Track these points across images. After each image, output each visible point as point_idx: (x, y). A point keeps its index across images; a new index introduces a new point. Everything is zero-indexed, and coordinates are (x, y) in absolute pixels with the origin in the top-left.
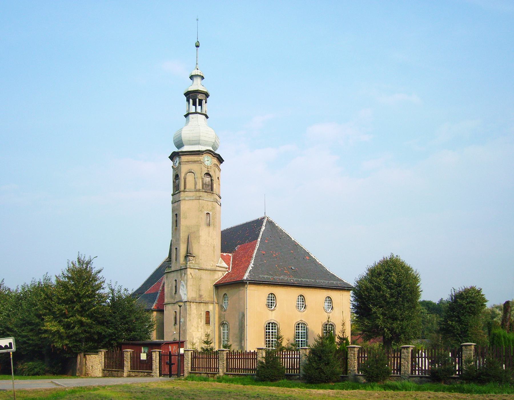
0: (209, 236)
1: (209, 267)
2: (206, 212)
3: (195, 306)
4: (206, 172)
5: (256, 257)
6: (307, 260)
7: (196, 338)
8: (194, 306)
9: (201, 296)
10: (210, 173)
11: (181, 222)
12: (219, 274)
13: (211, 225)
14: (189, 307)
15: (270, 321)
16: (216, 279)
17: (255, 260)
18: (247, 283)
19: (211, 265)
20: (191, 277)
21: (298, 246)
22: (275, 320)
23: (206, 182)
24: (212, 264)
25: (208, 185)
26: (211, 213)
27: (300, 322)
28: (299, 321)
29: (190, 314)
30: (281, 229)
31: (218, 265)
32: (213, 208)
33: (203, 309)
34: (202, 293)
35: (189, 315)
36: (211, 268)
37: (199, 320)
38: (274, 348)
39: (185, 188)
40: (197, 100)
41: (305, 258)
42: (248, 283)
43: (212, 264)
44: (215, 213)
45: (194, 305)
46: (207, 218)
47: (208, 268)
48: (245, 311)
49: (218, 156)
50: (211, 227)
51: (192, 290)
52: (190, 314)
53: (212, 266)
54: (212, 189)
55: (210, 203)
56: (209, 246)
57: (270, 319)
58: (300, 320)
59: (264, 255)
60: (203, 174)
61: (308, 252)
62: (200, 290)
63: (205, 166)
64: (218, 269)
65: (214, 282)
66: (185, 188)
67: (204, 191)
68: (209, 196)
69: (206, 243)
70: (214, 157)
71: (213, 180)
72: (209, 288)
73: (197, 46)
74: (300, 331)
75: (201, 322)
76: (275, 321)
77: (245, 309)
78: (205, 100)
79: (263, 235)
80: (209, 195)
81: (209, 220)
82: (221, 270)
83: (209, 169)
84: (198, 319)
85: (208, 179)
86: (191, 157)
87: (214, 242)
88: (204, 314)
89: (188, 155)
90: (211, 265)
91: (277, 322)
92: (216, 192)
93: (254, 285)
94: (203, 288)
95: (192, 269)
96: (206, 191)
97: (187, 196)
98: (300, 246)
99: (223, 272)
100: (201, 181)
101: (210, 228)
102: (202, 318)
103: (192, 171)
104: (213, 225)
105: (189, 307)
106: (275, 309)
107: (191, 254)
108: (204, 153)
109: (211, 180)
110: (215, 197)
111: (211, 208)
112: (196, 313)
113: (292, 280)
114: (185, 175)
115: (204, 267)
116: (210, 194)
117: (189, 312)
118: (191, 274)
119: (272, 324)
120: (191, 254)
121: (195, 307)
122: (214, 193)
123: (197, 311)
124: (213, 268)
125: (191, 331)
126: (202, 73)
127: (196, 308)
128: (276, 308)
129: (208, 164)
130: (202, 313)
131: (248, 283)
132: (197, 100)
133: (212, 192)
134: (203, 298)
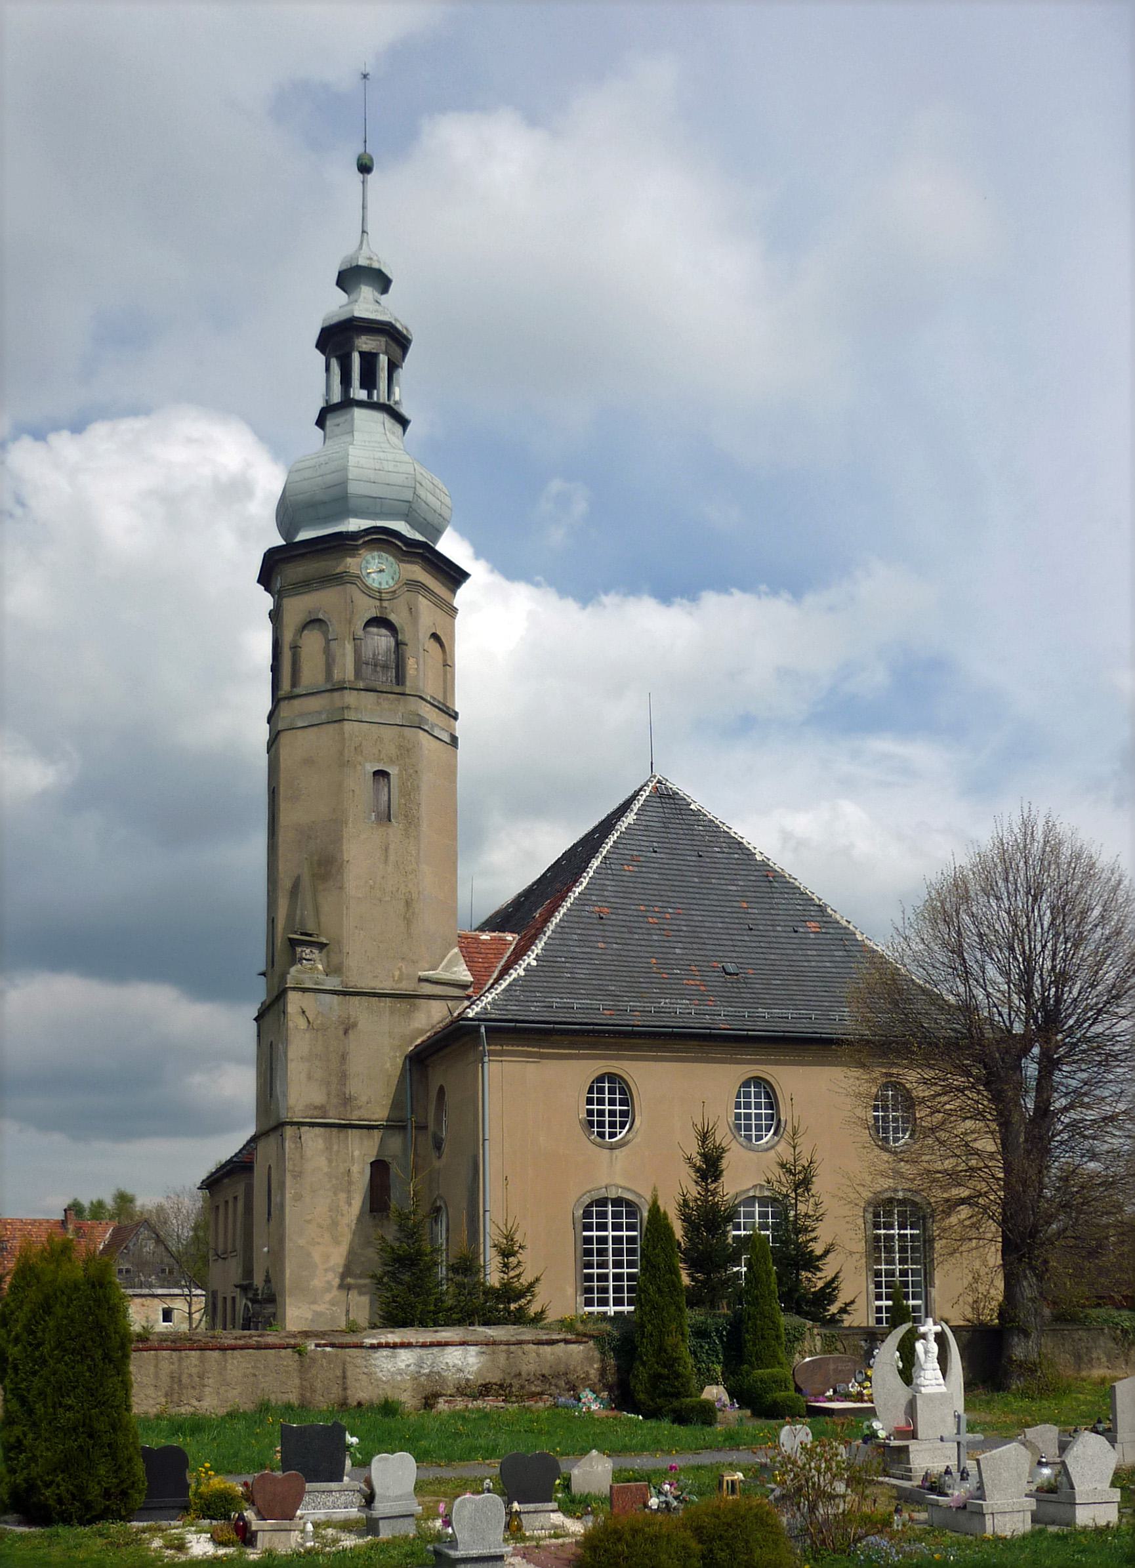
0: (386, 861)
1: (386, 986)
2: (371, 768)
3: (320, 1141)
4: (374, 613)
5: (559, 930)
6: (812, 936)
7: (326, 1270)
8: (314, 1140)
9: (347, 1101)
10: (392, 617)
11: (281, 818)
12: (433, 1011)
13: (396, 818)
14: (293, 1146)
15: (603, 1193)
16: (418, 1029)
17: (551, 944)
18: (478, 1031)
19: (393, 977)
20: (302, 1023)
21: (776, 884)
22: (627, 1185)
23: (374, 655)
24: (400, 969)
25: (385, 667)
26: (393, 771)
27: (751, 1194)
28: (748, 1190)
29: (301, 1172)
30: (712, 821)
31: (439, 973)
32: (406, 752)
33: (356, 1153)
34: (355, 1087)
35: (295, 1177)
36: (396, 986)
37: (342, 1196)
38: (626, 1309)
39: (295, 683)
40: (356, 359)
41: (801, 930)
42: (483, 1030)
43: (400, 969)
44: (412, 771)
45: (316, 1136)
46: (377, 792)
47: (381, 986)
48: (481, 1152)
49: (421, 551)
50: (397, 826)
51: (309, 1078)
52: (298, 1175)
53: (400, 980)
54: (400, 678)
55: (388, 733)
56: (388, 899)
57: (603, 1184)
58: (755, 1186)
59: (603, 921)
60: (359, 623)
61: (820, 906)
62: (343, 1077)
63: (368, 591)
64: (428, 989)
65: (411, 1043)
66: (295, 683)
67: (361, 685)
68: (386, 705)
69: (372, 887)
70: (406, 553)
71: (406, 645)
72: (388, 1065)
73: (365, 168)
74: (610, 1233)
75: (350, 1205)
76: (629, 1190)
77: (481, 1143)
78: (386, 353)
79: (620, 846)
80: (386, 702)
81: (386, 798)
82: (440, 993)
83: (385, 604)
84: (335, 1194)
85: (381, 641)
86: (316, 565)
87: (410, 885)
88: (362, 1173)
89: (303, 555)
90: (397, 973)
91: (639, 1196)
92: (418, 689)
93: (620, 1047)
94: (358, 1064)
95: (306, 994)
96: (373, 685)
97: (301, 715)
98: (789, 882)
99: (450, 1003)
100: (349, 648)
101: (390, 831)
102: (353, 1187)
103: (321, 616)
104: (406, 816)
105: (296, 1143)
106: (628, 1142)
107: (310, 935)
108: (361, 542)
109: (398, 644)
110: (412, 707)
111: (392, 750)
112: (326, 1170)
113: (722, 1017)
114: (295, 635)
115: (366, 984)
116: (390, 696)
117: (294, 1165)
118: (304, 1012)
119: (617, 1202)
120: (310, 935)
121: (320, 1144)
122: (408, 692)
123: (330, 1161)
124: (406, 986)
125: (301, 1242)
126: (375, 258)
127: (328, 1148)
128: (630, 1136)
129: (380, 584)
130: (355, 1169)
131: (483, 1030)
132: (356, 359)
133: (398, 689)
134: (360, 1108)
